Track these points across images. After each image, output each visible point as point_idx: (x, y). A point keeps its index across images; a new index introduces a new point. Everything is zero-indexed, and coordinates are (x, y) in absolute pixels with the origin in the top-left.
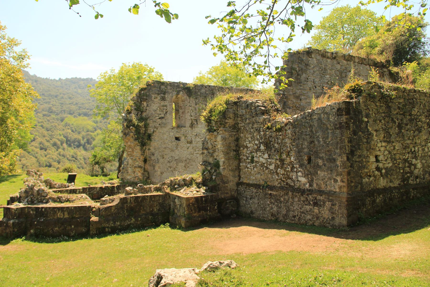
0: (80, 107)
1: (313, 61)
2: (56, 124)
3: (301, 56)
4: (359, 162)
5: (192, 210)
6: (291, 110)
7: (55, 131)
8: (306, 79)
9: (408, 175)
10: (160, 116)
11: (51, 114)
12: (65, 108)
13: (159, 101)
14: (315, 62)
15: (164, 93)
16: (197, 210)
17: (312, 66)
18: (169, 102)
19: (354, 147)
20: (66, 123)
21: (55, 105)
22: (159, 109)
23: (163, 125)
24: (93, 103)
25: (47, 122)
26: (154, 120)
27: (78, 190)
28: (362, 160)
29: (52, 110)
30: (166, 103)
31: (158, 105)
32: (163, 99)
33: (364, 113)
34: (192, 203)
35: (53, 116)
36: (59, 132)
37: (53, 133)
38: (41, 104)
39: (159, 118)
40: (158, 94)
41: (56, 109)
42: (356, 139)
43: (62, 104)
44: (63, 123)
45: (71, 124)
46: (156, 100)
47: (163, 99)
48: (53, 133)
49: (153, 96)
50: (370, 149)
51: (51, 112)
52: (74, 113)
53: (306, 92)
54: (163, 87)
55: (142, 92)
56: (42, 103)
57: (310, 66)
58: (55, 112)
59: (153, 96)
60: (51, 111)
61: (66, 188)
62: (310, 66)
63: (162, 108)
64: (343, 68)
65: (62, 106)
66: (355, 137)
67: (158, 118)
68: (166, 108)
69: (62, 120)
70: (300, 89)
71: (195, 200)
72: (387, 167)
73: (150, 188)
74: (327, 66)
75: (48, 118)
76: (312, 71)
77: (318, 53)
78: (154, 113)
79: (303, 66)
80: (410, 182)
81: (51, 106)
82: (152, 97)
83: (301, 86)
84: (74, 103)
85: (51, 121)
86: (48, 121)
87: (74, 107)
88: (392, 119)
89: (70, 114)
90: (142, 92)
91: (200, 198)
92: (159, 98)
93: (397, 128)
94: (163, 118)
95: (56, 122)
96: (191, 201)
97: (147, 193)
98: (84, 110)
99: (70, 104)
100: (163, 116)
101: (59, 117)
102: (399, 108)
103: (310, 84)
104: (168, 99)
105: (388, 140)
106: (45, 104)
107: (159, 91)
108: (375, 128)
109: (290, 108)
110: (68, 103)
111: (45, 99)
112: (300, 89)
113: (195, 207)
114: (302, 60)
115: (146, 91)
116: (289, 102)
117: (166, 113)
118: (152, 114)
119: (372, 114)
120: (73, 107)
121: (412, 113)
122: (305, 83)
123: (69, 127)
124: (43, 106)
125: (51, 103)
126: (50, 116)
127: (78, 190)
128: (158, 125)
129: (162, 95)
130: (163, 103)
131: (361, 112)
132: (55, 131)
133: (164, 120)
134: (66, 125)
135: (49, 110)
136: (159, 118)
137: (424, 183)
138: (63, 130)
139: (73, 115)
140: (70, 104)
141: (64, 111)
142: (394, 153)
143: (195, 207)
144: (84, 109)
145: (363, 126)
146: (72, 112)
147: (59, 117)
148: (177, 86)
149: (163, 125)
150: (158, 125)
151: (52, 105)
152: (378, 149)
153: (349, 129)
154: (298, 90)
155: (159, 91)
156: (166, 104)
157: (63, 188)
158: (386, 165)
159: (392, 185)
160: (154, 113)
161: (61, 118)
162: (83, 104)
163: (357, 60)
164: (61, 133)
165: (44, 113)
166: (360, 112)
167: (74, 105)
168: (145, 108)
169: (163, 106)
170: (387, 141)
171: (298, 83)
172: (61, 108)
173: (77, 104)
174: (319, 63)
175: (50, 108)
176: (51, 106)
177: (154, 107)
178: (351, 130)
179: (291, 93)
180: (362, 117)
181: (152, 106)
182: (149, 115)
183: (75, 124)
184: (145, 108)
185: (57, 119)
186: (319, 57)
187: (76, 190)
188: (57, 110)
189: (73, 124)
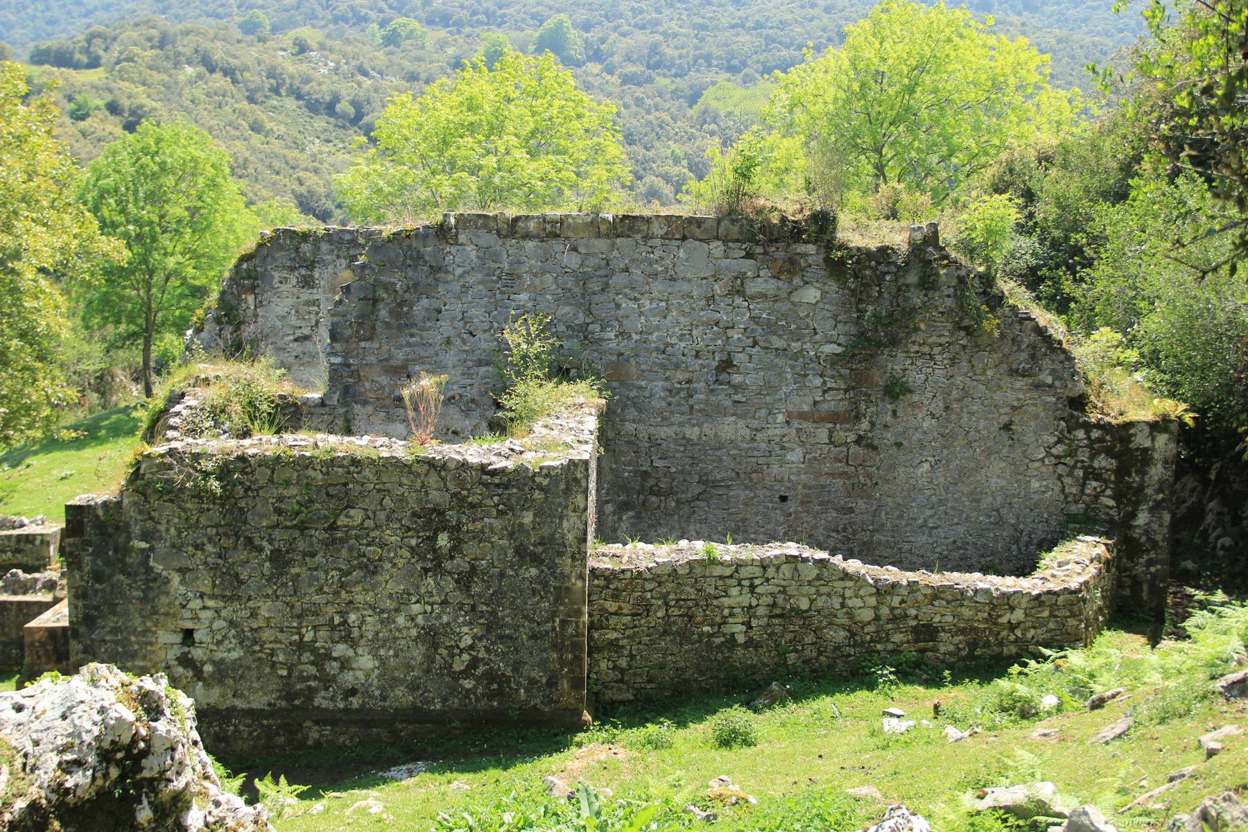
0: (770, 40)
1: (466, 252)
2: (667, 118)
3: (414, 243)
4: (116, 642)
5: (39, 657)
6: (370, 409)
7: (657, 144)
8: (434, 314)
9: (312, 684)
10: (299, 333)
11: (654, 75)
12: (710, 47)
13: (295, 290)
14: (473, 255)
15: (311, 266)
16: (54, 658)
17: (459, 271)
18: (324, 292)
19: (97, 608)
20: (705, 111)
21: (675, 35)
22: (293, 312)
23: (306, 359)
24: (826, 19)
25: (634, 108)
26: (280, 344)
27: (39, 538)
28: (127, 639)
29: (662, 54)
30: (317, 294)
31: (290, 301)
32: (307, 282)
33: (136, 530)
34: (39, 641)
35: (662, 82)
36: (673, 146)
37: (650, 154)
38: (624, 35)
39: (296, 340)
40: (292, 269)
41: (676, 53)
42: (102, 590)
43: (704, 28)
44: (693, 112)
45: (722, 113)
46: (284, 287)
47: (307, 282)
48: (650, 154)
49: (276, 275)
50: (156, 613)
51: (657, 65)
52: (744, 64)
53: (431, 351)
54: (306, 248)
55: (245, 266)
56: (626, 28)
57: (447, 272)
58: (673, 65)
59: (276, 275)
60: (655, 61)
61: (14, 528)
62: (447, 272)
63: (303, 309)
64: (593, 262)
65: (702, 40)
66: (97, 586)
67: (291, 338)
68: (316, 308)
69: (693, 100)
70: (409, 344)
71: (46, 634)
72: (222, 660)
73: (36, 580)
74: (519, 263)
75: (639, 92)
76: (457, 287)
77: (485, 226)
78: (279, 323)
79: (421, 275)
80: (317, 702)
81: (659, 38)
82: (273, 278)
83: (412, 335)
84: (749, 24)
85: (648, 101)
86: (639, 102)
87: (748, 38)
88: (249, 541)
89: (732, 69)
90: (245, 266)
91: (60, 633)
92: (294, 282)
93: (267, 564)
94: (306, 338)
95: (667, 105)
96: (37, 637)
97: (25, 593)
98: (784, 53)
99: (733, 27)
100: (306, 331)
101: (682, 84)
102: (279, 511)
103: (445, 327)
104: (322, 283)
105: (230, 586)
106: (637, 31)
107: (293, 260)
108: (177, 565)
109: (365, 403)
110: (725, 22)
111: (642, 11)
112: (409, 344)
113: (46, 650)
114: (420, 256)
115: (257, 261)
116: (367, 385)
117: (317, 323)
118: (273, 327)
119: (168, 530)
120: (745, 41)
121: (339, 523)
122: (428, 324)
123: (713, 127)
124: (628, 40)
125: (661, 29)
126: (650, 80)
127: (39, 538)
128: (291, 360)
129: (303, 272)
130: (306, 295)
131: (127, 525)
132: (657, 144)
133: (308, 345)
134: (707, 117)
135: (650, 57)
136: (296, 340)
137: (384, 709)
138: (691, 138)
139: (739, 77)
140: (733, 27)
141: (708, 58)
142: (255, 626)
143: (46, 650)
144: (788, 47)
145: (132, 559)
146: (735, 62)
147: (682, 84)
148: (349, 242)
149: (306, 359)
150: (291, 360)
151: (665, 34)
152: (187, 614)
153: (80, 568)
154: (400, 347)
155: (293, 260)
156: (316, 297)
157: (8, 528)
158: (219, 655)
159: (240, 704)
160: (279, 323)
161: (691, 87)
162: (783, 25)
163: (658, 229)
164: (678, 149)
165: (631, 69)
166: (124, 528)
167: (748, 30)
168: (250, 313)
169: (307, 303)
170: (224, 597)
171: (400, 328)
172: (696, 48)
173: (758, 26)
174: (486, 254)
175: (654, 49)
176: (659, 38)
177: (278, 309)
178: (87, 569)
179: (373, 359)
180: (129, 539)
181: (273, 305)
182: (266, 331)
183: (737, 112)
184: (250, 313)
185: (674, 92)
186: (488, 239)
187: (34, 536)
188: (680, 57)
189: (729, 114)
